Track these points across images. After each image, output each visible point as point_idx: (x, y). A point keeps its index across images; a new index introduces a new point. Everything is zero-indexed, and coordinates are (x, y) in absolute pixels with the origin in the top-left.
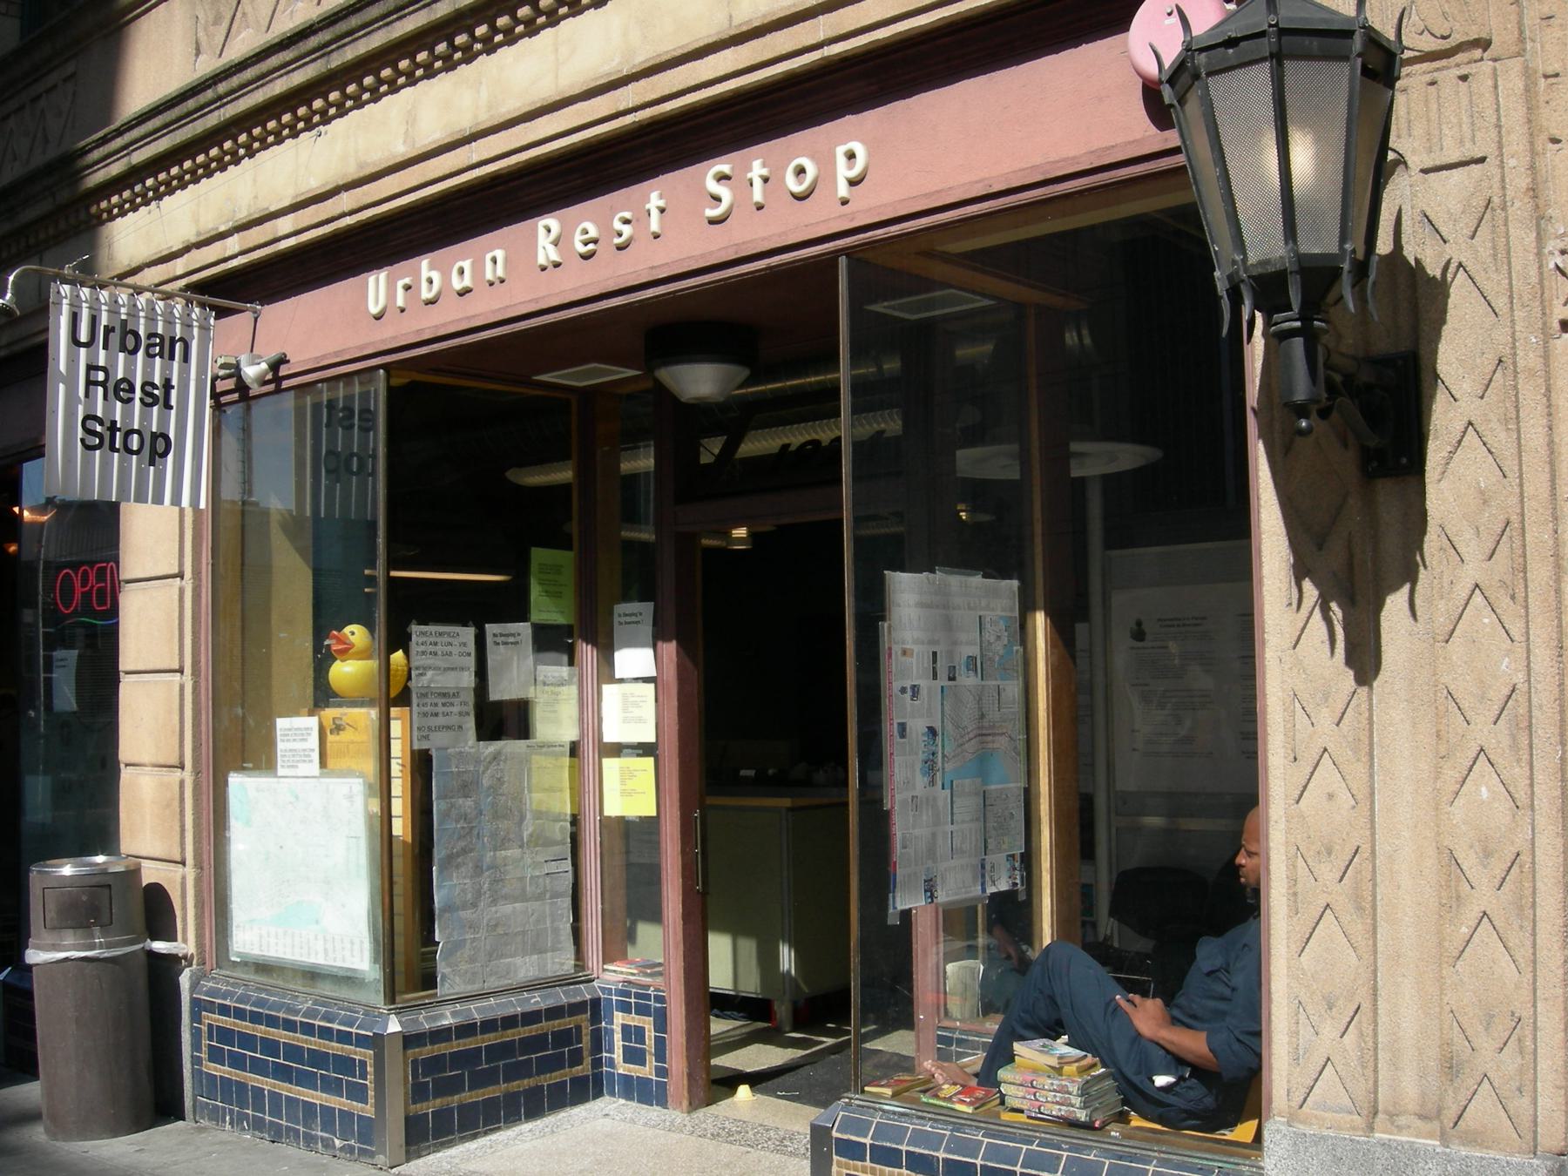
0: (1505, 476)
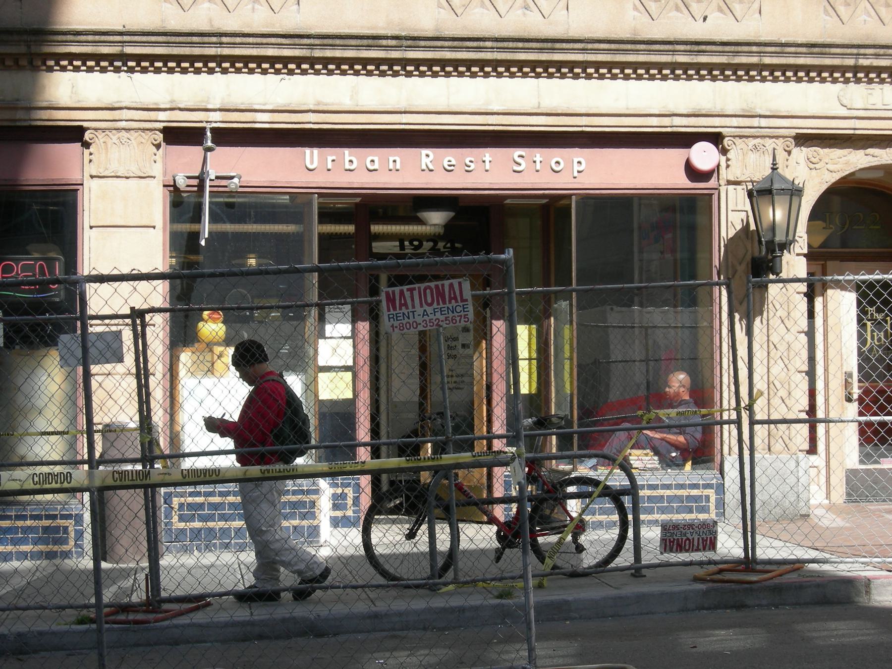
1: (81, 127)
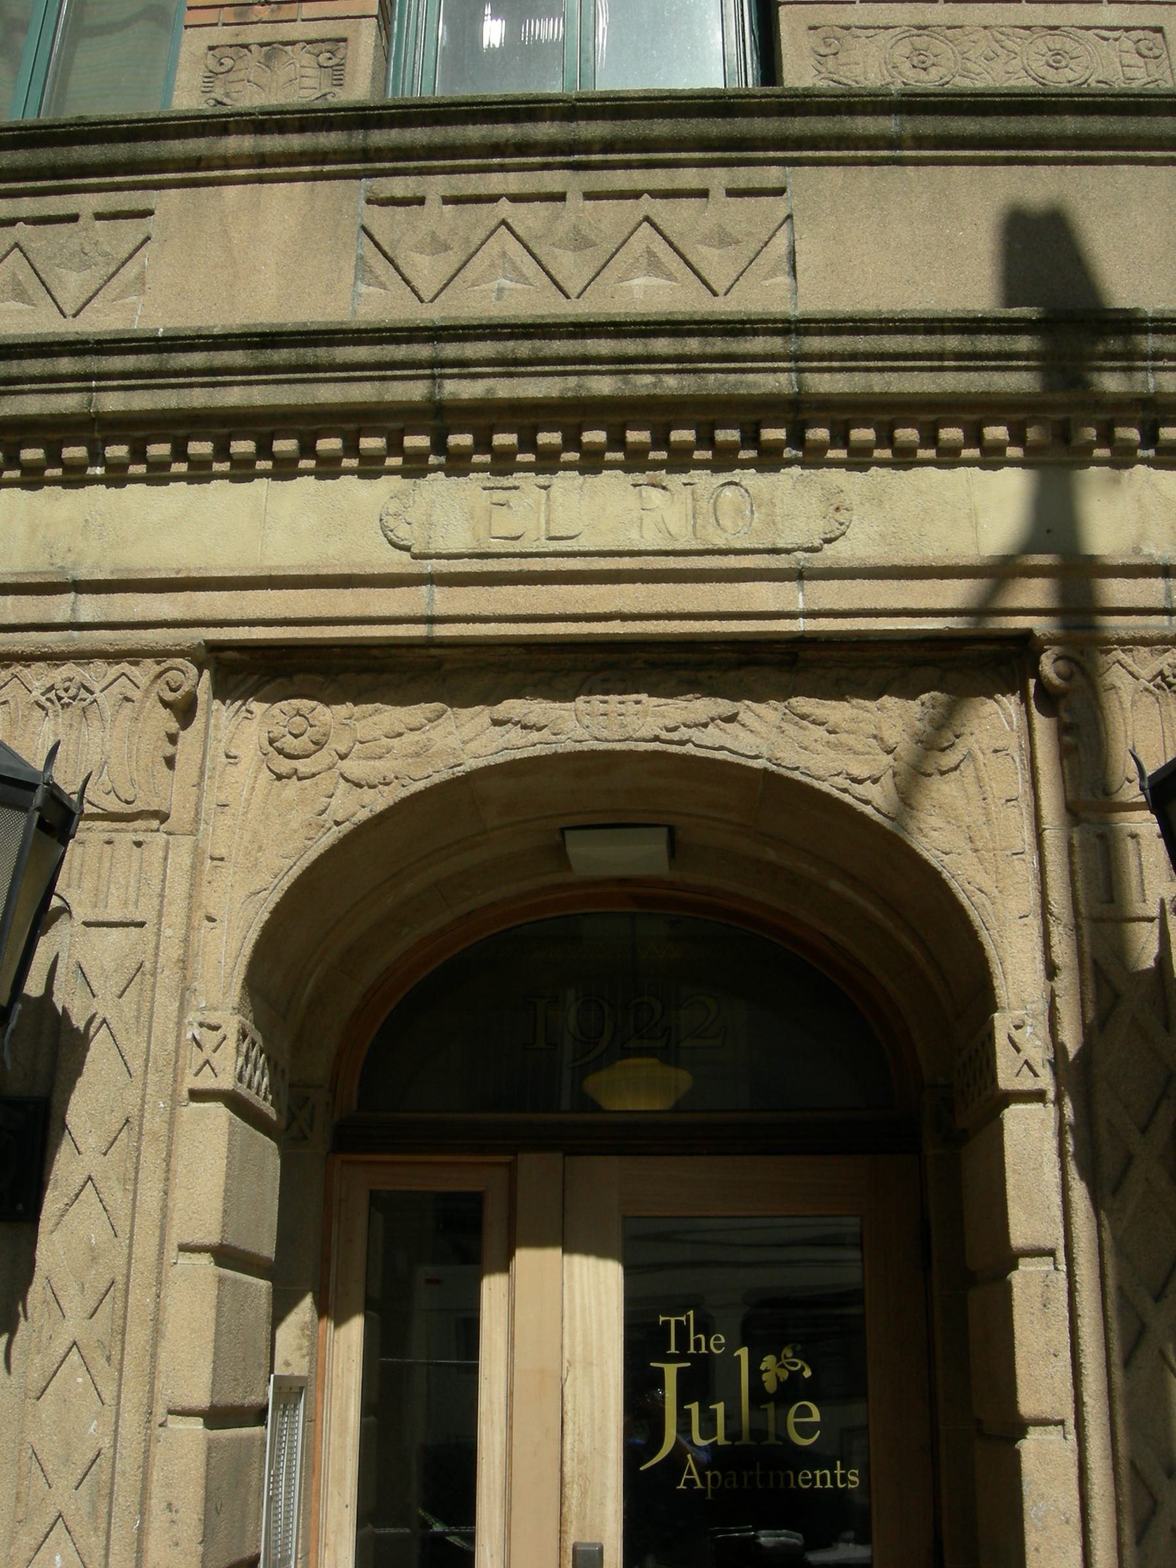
0: (116, 1236)
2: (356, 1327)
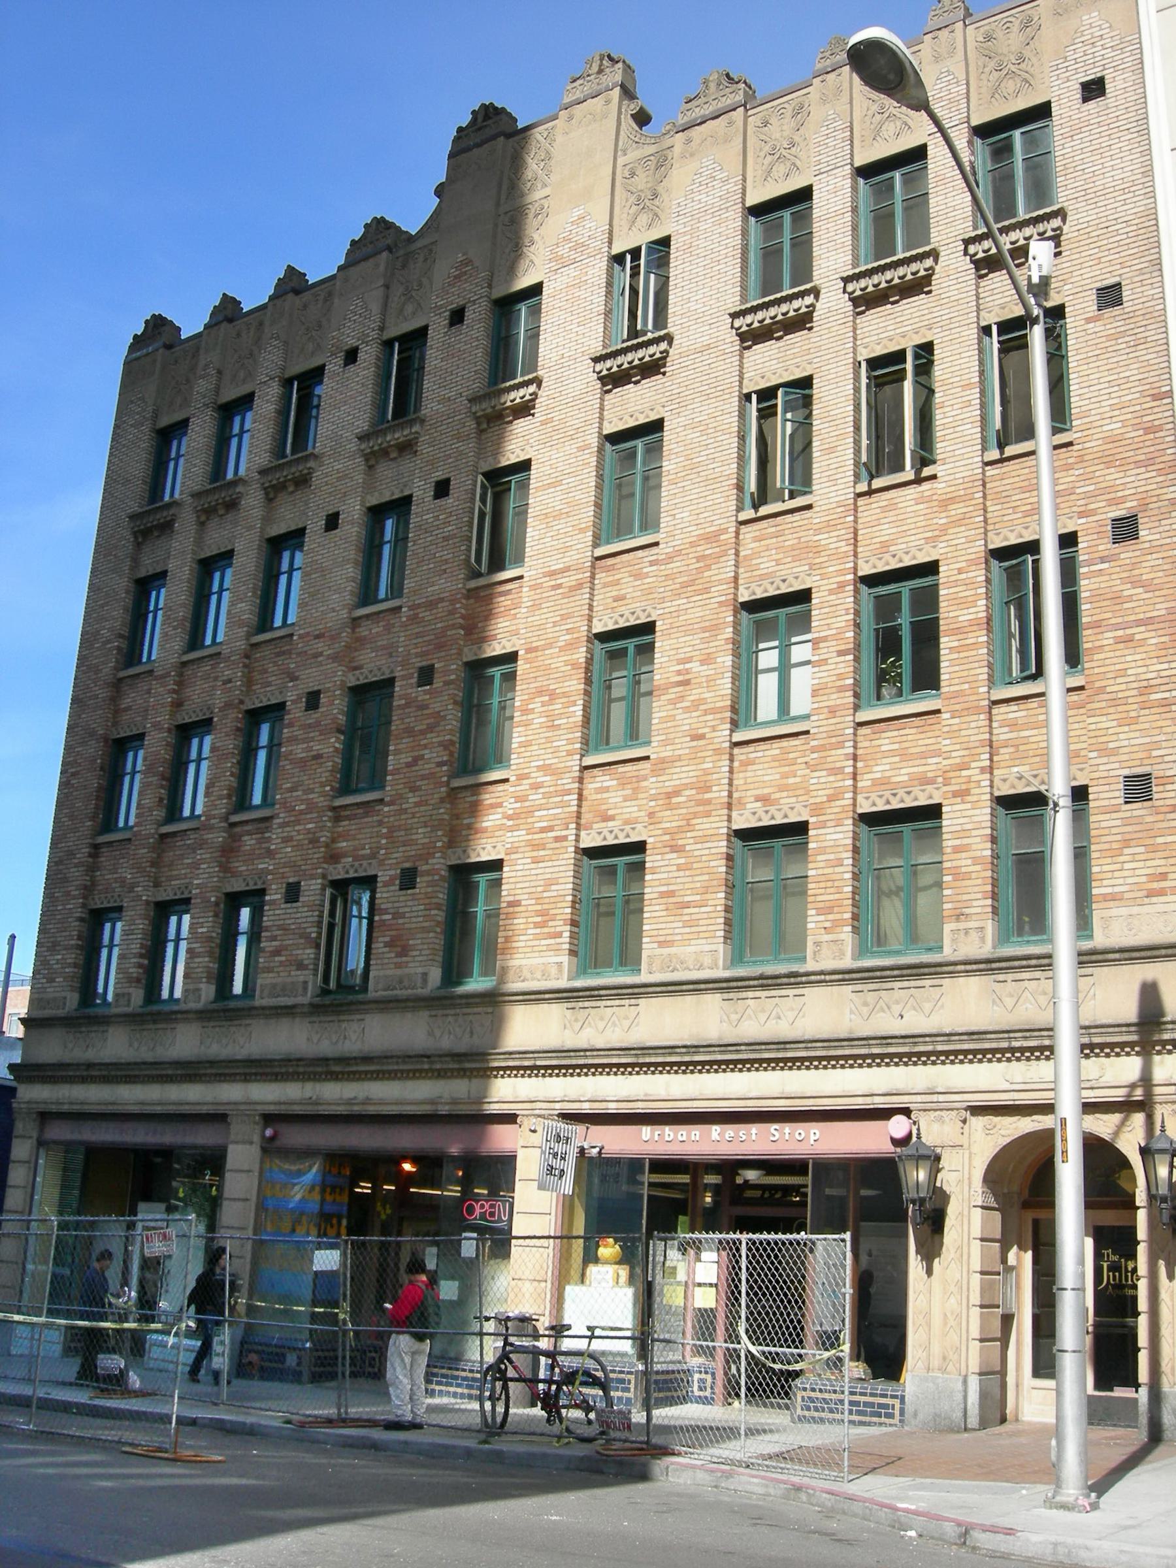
1: (908, 1108)
2: (1030, 1253)
